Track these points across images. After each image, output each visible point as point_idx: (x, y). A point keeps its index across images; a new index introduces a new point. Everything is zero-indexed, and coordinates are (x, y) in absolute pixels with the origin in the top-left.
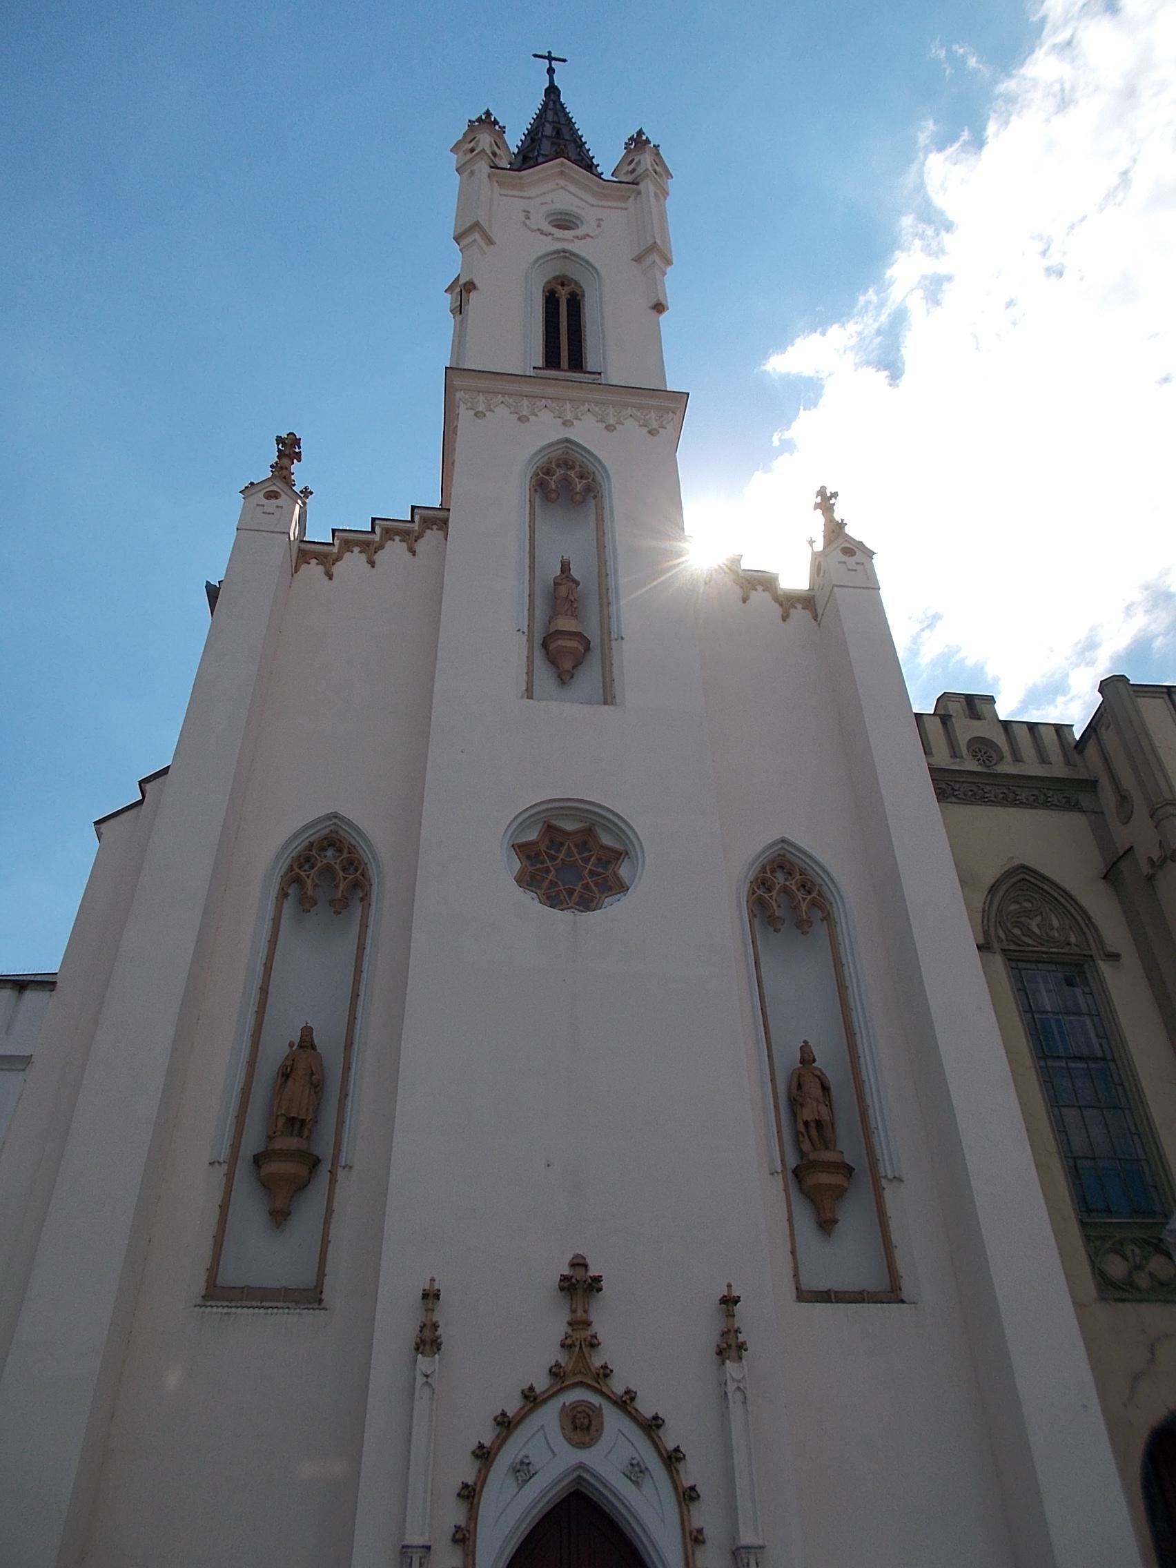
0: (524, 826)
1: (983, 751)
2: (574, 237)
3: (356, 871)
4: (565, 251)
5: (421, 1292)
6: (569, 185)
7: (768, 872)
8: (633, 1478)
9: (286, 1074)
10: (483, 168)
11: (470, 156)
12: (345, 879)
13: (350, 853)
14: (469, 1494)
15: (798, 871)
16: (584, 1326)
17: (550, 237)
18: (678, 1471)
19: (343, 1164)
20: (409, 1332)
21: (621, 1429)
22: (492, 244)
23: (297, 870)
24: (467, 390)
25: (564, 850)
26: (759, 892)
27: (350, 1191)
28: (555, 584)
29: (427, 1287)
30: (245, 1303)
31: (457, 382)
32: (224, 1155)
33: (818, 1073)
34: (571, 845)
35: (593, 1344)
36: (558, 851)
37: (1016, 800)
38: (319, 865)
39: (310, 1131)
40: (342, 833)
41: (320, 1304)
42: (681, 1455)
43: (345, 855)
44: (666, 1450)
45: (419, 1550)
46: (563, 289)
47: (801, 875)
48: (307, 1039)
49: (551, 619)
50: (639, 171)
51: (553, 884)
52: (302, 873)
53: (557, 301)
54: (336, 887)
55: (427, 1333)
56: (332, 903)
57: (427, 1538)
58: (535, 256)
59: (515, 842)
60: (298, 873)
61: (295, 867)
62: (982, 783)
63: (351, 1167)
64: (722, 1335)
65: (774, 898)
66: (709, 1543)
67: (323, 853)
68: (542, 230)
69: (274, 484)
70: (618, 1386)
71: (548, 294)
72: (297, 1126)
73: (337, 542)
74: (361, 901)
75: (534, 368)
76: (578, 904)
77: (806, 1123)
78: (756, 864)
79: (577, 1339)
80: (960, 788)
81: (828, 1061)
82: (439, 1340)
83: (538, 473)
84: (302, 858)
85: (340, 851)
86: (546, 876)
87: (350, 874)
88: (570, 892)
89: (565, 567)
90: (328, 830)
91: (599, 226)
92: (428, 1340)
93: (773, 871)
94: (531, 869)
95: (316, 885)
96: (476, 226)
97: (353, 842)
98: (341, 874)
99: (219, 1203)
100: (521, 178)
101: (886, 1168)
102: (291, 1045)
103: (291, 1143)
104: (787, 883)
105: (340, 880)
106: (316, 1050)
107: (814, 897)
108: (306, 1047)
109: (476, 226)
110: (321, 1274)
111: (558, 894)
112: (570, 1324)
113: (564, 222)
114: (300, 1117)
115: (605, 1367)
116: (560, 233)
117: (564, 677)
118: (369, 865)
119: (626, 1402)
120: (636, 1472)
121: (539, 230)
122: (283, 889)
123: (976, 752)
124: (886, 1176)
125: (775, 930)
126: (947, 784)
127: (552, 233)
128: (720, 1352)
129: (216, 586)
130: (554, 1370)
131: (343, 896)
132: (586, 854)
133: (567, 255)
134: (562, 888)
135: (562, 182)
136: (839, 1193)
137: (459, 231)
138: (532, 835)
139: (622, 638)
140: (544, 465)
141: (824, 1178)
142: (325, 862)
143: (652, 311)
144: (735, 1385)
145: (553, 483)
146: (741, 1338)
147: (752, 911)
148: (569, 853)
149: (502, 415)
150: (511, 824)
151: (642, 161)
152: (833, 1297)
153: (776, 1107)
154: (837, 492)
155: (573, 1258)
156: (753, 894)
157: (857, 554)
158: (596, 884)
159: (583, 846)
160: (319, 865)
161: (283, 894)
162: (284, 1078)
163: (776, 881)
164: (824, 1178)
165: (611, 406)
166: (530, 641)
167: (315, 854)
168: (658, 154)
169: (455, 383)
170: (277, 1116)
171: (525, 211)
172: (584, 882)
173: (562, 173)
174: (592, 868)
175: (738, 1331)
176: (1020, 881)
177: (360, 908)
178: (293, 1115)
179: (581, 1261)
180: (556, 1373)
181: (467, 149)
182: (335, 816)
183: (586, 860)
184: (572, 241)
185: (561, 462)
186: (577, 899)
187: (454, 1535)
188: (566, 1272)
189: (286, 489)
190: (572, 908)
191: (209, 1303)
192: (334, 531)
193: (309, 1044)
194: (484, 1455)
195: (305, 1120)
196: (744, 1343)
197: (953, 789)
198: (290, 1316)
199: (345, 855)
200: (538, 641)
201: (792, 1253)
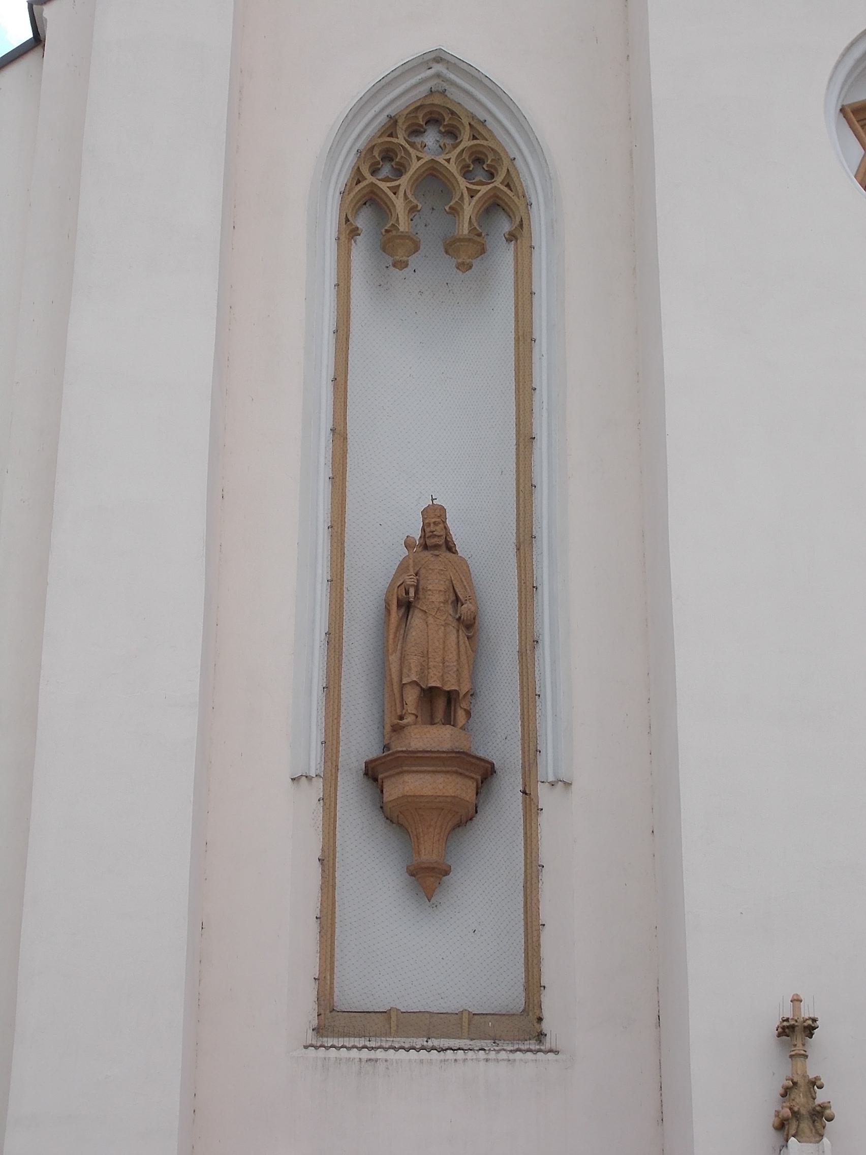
3: (492, 175)
5: (777, 1023)
13: (474, 138)
15: (468, 127)
23: (370, 179)
29: (789, 1015)
30: (398, 1042)
32: (314, 763)
38: (415, 165)
39: (468, 713)
40: (454, 94)
41: (540, 1042)
43: (466, 142)
48: (439, 530)
52: (384, 186)
54: (455, 211)
56: (451, 246)
59: (847, 102)
60: (372, 183)
61: (366, 172)
63: (568, 785)
64: (784, 1095)
67: (418, 140)
72: (441, 704)
74: (509, 240)
82: (828, 1112)
84: (376, 153)
85: (452, 133)
87: (481, 183)
90: (424, 89)
92: (803, 1111)
95: (413, 210)
97: (481, 115)
98: (463, 184)
99: (318, 854)
102: (408, 544)
104: (441, 159)
106: (455, 552)
108: (436, 547)
114: (447, 688)
118: (519, 163)
122: (347, 220)
128: (781, 1126)
131: (472, 230)
142: (426, 158)
146: (821, 1097)
150: (839, 62)
160: (415, 165)
162: (403, 610)
167: (403, 143)
170: (403, 686)
175: (814, 1084)
178: (433, 684)
182: (438, 57)
191: (330, 1042)
193: (441, 541)
195: (457, 692)
196: (824, 1107)
198: (490, 1064)
199: (466, 142)
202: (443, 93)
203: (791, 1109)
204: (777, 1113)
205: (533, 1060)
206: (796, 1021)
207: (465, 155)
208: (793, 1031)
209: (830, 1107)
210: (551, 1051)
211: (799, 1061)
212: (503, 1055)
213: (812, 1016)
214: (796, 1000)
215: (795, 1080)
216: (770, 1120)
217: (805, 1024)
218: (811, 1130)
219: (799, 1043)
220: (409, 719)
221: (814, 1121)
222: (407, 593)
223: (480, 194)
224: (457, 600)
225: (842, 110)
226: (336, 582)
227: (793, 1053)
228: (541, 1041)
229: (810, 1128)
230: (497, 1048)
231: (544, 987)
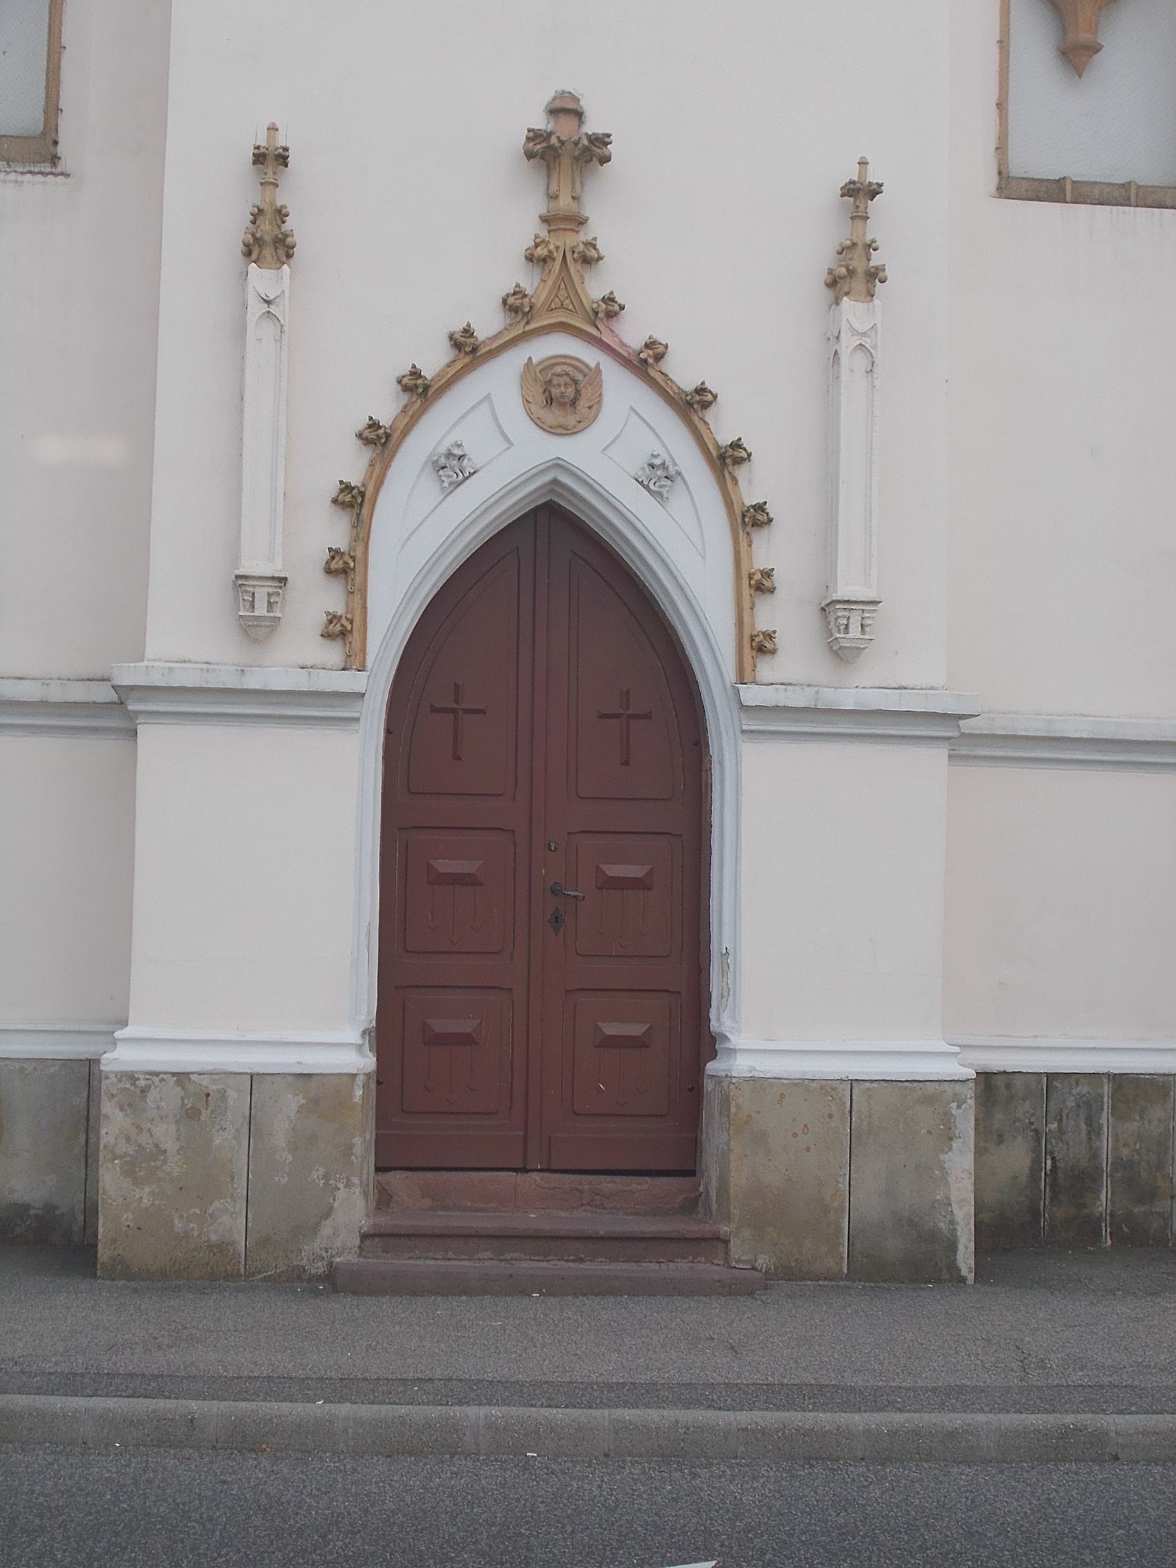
35: (589, 259)
41: (54, 164)
42: (744, 454)
55: (266, 227)
92: (267, 238)
110: (52, 110)
128: (833, 283)
146: (876, 259)
175: (870, 247)
179: (571, 105)
203: (253, 235)
204: (830, 272)
205: (40, 182)
206: (267, 149)
208: (265, 159)
209: (293, 236)
210: (62, 174)
211: (859, 223)
212: (13, 176)
213: (284, 145)
214: (273, 129)
215: (261, 207)
216: (824, 276)
217: (276, 153)
218: (273, 257)
219: (270, 171)
221: (276, 248)
227: (263, 181)
228: (55, 164)
229: (272, 254)
230: (8, 169)
231: (61, 110)
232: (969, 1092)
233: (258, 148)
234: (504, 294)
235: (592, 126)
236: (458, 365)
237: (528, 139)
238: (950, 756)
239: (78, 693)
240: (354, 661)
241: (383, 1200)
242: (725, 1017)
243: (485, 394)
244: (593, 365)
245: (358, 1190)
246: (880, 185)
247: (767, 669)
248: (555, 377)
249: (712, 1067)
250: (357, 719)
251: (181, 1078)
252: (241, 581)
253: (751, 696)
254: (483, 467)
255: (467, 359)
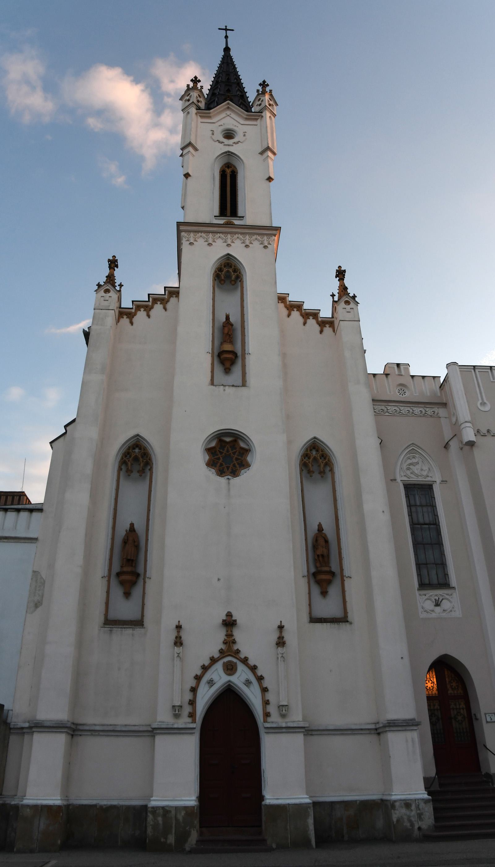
0: (210, 441)
1: (402, 390)
2: (233, 143)
4: (229, 152)
6: (232, 114)
7: (309, 451)
8: (246, 684)
9: (125, 542)
10: (193, 110)
11: (188, 103)
12: (143, 461)
14: (194, 690)
16: (231, 637)
17: (223, 144)
18: (261, 683)
19: (147, 577)
20: (172, 637)
21: (243, 669)
22: (197, 150)
23: (125, 459)
24: (185, 231)
25: (226, 449)
26: (305, 460)
27: (151, 587)
28: (223, 326)
31: (182, 228)
33: (323, 535)
34: (229, 447)
35: (234, 642)
36: (223, 450)
37: (413, 413)
42: (263, 678)
43: (321, 453)
44: (258, 676)
45: (178, 707)
46: (228, 170)
47: (322, 452)
49: (222, 344)
50: (263, 105)
51: (221, 465)
53: (226, 176)
55: (178, 639)
56: (320, 473)
57: (180, 703)
58: (215, 157)
59: (207, 448)
62: (400, 406)
63: (150, 578)
65: (310, 462)
66: (271, 704)
67: (134, 451)
68: (219, 141)
69: (108, 285)
70: (242, 656)
71: (222, 173)
73: (134, 307)
75: (215, 216)
76: (231, 473)
77: (318, 556)
78: (303, 450)
79: (228, 641)
80: (390, 408)
81: (329, 531)
83: (216, 271)
86: (219, 461)
88: (228, 468)
89: (228, 317)
91: (244, 136)
93: (311, 450)
94: (213, 458)
96: (190, 144)
100: (210, 113)
101: (346, 573)
102: (126, 531)
103: (127, 569)
104: (316, 456)
105: (141, 462)
107: (326, 461)
109: (190, 144)
110: (143, 616)
111: (223, 469)
112: (226, 635)
113: (229, 135)
115: (238, 650)
116: (226, 141)
117: (227, 371)
118: (152, 455)
119: (245, 661)
120: (248, 683)
121: (218, 140)
122: (120, 467)
123: (399, 390)
124: (345, 576)
125: (310, 476)
126: (385, 407)
127: (224, 142)
128: (277, 644)
129: (87, 331)
130: (220, 651)
132: (234, 451)
133: (230, 153)
134: (225, 466)
135: (228, 112)
136: (329, 582)
137: (183, 146)
138: (213, 444)
139: (250, 354)
140: (219, 267)
141: (324, 577)
143: (266, 181)
144: (281, 655)
145: (222, 275)
147: (301, 468)
148: (228, 451)
149: (201, 243)
151: (264, 100)
152: (323, 620)
153: (307, 550)
154: (345, 270)
155: (227, 613)
156: (302, 461)
157: (351, 303)
158: (238, 464)
159: (233, 447)
161: (120, 469)
163: (312, 455)
164: (324, 577)
165: (247, 235)
166: (213, 357)
168: (271, 95)
169: (180, 229)
171: (212, 131)
172: (233, 463)
173: (228, 108)
174: (237, 457)
176: (412, 450)
177: (149, 474)
179: (230, 614)
180: (221, 651)
181: (186, 100)
182: (138, 435)
183: (234, 453)
184: (232, 145)
185: (226, 264)
186: (231, 471)
187: (189, 702)
188: (225, 618)
189: (113, 289)
190: (228, 475)
192: (133, 301)
194: (198, 678)
197: (387, 409)
200: (216, 353)
201: (309, 605)
202: (139, 442)
207: (321, 455)
220: (124, 565)
222: (125, 540)
223: (144, 462)
224: (135, 542)
225: (206, 449)
226: (113, 539)
232: (311, 805)
233: (176, 625)
234: (219, 649)
235: (234, 618)
236: (204, 672)
237: (223, 621)
238: (304, 735)
239: (145, 728)
240: (194, 721)
241: (201, 834)
242: (264, 792)
243: (216, 669)
244: (235, 662)
245: (195, 831)
246: (284, 626)
247: (269, 719)
248: (411, 459)
249: (263, 803)
250: (194, 733)
251: (163, 808)
252: (174, 706)
253: (267, 725)
254: (216, 682)
255: (213, 662)
